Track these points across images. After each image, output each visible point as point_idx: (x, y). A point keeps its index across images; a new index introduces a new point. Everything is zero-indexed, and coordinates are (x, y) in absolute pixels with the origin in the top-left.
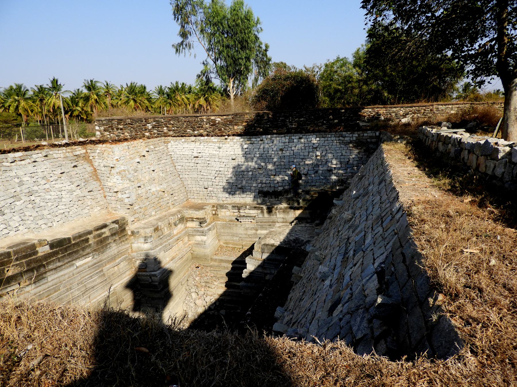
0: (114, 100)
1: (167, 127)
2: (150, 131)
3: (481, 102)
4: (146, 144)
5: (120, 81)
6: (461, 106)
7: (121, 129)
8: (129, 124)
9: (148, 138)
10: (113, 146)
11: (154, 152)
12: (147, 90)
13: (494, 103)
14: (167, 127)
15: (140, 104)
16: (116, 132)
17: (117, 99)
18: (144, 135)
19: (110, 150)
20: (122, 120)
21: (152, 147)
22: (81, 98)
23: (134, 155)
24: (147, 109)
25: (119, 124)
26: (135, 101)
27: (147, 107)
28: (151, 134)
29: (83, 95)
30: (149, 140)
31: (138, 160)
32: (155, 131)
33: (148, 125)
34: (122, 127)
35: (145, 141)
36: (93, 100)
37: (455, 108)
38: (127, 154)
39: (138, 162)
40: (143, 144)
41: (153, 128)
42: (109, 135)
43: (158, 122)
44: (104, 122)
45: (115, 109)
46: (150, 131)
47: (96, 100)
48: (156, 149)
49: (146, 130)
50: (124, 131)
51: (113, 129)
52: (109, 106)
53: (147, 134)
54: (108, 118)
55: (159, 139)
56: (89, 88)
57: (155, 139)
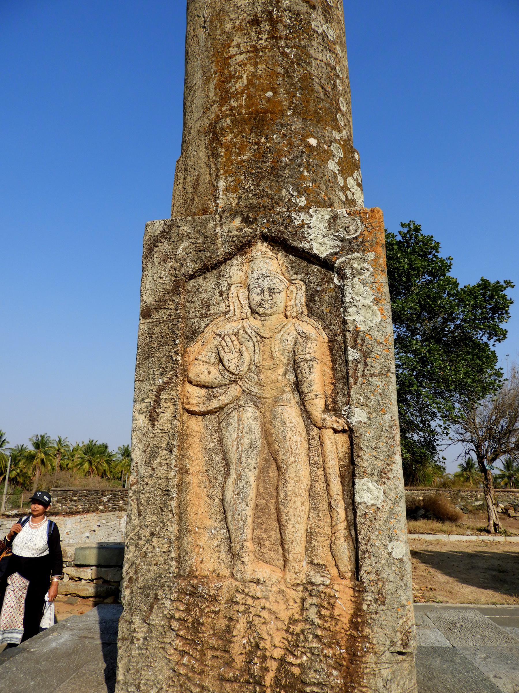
0: (64, 460)
1: (124, 500)
2: (105, 504)
3: (447, 489)
4: (99, 519)
5: (76, 437)
6: (426, 492)
7: (75, 501)
8: (85, 496)
9: (102, 512)
10: (65, 518)
11: (105, 527)
12: (109, 450)
13: (459, 491)
14: (124, 500)
15: (96, 467)
16: (69, 504)
17: (68, 459)
18: (97, 508)
19: (62, 522)
20: (77, 491)
21: (104, 521)
22: (25, 457)
23: (84, 529)
24: (103, 475)
25: (74, 495)
26: (90, 462)
27: (105, 471)
28: (105, 508)
29: (26, 454)
30: (102, 514)
31: (87, 534)
32: (110, 505)
33: (104, 497)
34: (76, 498)
35: (98, 515)
36: (39, 460)
37: (421, 493)
38: (78, 527)
39: (88, 537)
40: (95, 518)
41: (108, 501)
42: (61, 507)
43: (114, 495)
44: (59, 493)
45: (63, 472)
46: (105, 504)
47: (42, 461)
48: (108, 524)
49: (101, 503)
50: (78, 503)
51: (66, 501)
52: (57, 468)
53: (101, 507)
54: (63, 489)
55: (112, 513)
56: (37, 446)
57: (109, 513)
